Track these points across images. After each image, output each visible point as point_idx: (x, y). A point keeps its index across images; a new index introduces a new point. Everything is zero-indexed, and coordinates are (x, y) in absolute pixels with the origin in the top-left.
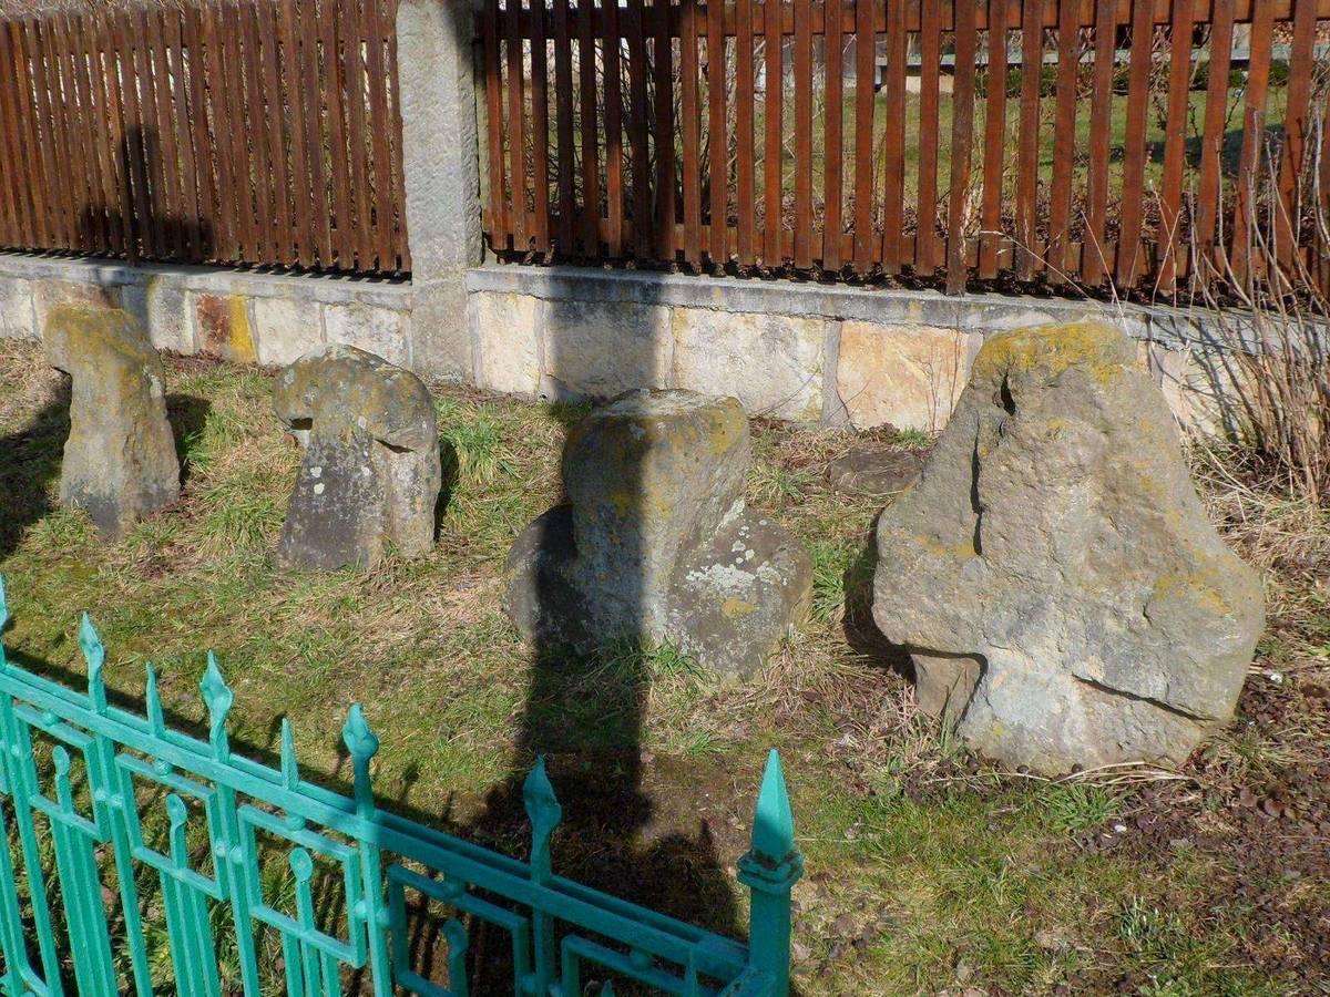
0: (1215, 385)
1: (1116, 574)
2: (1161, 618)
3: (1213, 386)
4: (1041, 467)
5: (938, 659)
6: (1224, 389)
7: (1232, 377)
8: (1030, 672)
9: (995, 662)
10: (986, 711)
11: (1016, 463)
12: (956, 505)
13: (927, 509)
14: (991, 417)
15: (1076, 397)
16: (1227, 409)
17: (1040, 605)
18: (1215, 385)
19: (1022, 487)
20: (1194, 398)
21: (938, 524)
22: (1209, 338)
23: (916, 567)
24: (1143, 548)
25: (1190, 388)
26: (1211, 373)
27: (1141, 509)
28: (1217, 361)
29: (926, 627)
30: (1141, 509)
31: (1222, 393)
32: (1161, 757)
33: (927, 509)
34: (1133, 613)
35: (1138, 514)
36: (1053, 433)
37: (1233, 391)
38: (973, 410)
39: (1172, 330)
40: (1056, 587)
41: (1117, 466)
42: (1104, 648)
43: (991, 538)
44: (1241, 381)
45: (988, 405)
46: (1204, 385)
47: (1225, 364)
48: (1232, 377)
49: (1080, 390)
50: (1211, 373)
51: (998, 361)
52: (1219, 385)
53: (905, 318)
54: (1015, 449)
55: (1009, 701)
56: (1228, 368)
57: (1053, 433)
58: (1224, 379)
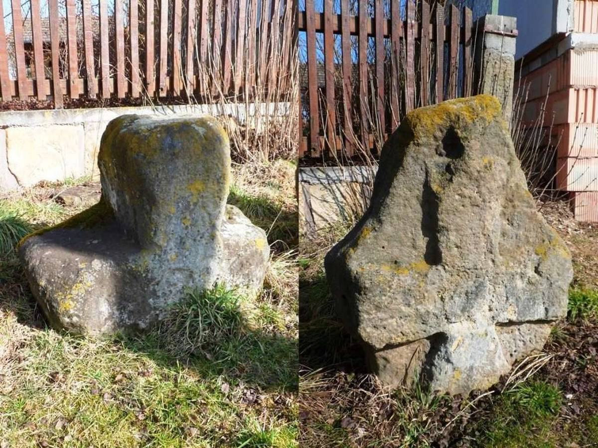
0: (335, 198)
1: (512, 254)
2: (546, 270)
3: (334, 199)
4: (484, 190)
5: (397, 349)
6: (339, 199)
7: (341, 193)
8: (473, 331)
9: (452, 333)
10: (448, 367)
11: (467, 192)
12: (410, 235)
13: (386, 244)
14: (437, 165)
15: (493, 140)
16: (342, 210)
17: (482, 284)
18: (335, 198)
19: (469, 208)
20: (327, 205)
21: (396, 252)
22: (329, 177)
23: (394, 287)
24: (526, 233)
25: (325, 201)
26: (332, 192)
27: (525, 209)
28: (334, 187)
29: (405, 327)
30: (525, 209)
31: (338, 201)
32: (532, 351)
33: (386, 244)
34: (531, 273)
35: (525, 213)
36: (488, 165)
37: (342, 199)
38: (420, 162)
39: (313, 175)
40: (490, 270)
41: (513, 185)
42: (517, 299)
43: (449, 249)
44: (345, 194)
45: (432, 157)
46: (330, 198)
47: (337, 188)
48: (341, 193)
49: (497, 135)
50: (332, 192)
51: (437, 120)
52: (337, 198)
53: (44, 121)
54: (465, 181)
55: (463, 355)
56: (339, 190)
57: (488, 165)
58: (338, 194)
